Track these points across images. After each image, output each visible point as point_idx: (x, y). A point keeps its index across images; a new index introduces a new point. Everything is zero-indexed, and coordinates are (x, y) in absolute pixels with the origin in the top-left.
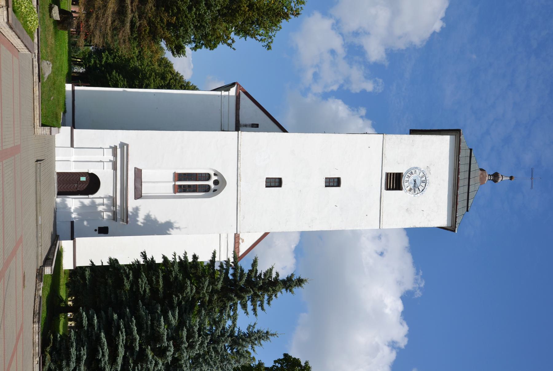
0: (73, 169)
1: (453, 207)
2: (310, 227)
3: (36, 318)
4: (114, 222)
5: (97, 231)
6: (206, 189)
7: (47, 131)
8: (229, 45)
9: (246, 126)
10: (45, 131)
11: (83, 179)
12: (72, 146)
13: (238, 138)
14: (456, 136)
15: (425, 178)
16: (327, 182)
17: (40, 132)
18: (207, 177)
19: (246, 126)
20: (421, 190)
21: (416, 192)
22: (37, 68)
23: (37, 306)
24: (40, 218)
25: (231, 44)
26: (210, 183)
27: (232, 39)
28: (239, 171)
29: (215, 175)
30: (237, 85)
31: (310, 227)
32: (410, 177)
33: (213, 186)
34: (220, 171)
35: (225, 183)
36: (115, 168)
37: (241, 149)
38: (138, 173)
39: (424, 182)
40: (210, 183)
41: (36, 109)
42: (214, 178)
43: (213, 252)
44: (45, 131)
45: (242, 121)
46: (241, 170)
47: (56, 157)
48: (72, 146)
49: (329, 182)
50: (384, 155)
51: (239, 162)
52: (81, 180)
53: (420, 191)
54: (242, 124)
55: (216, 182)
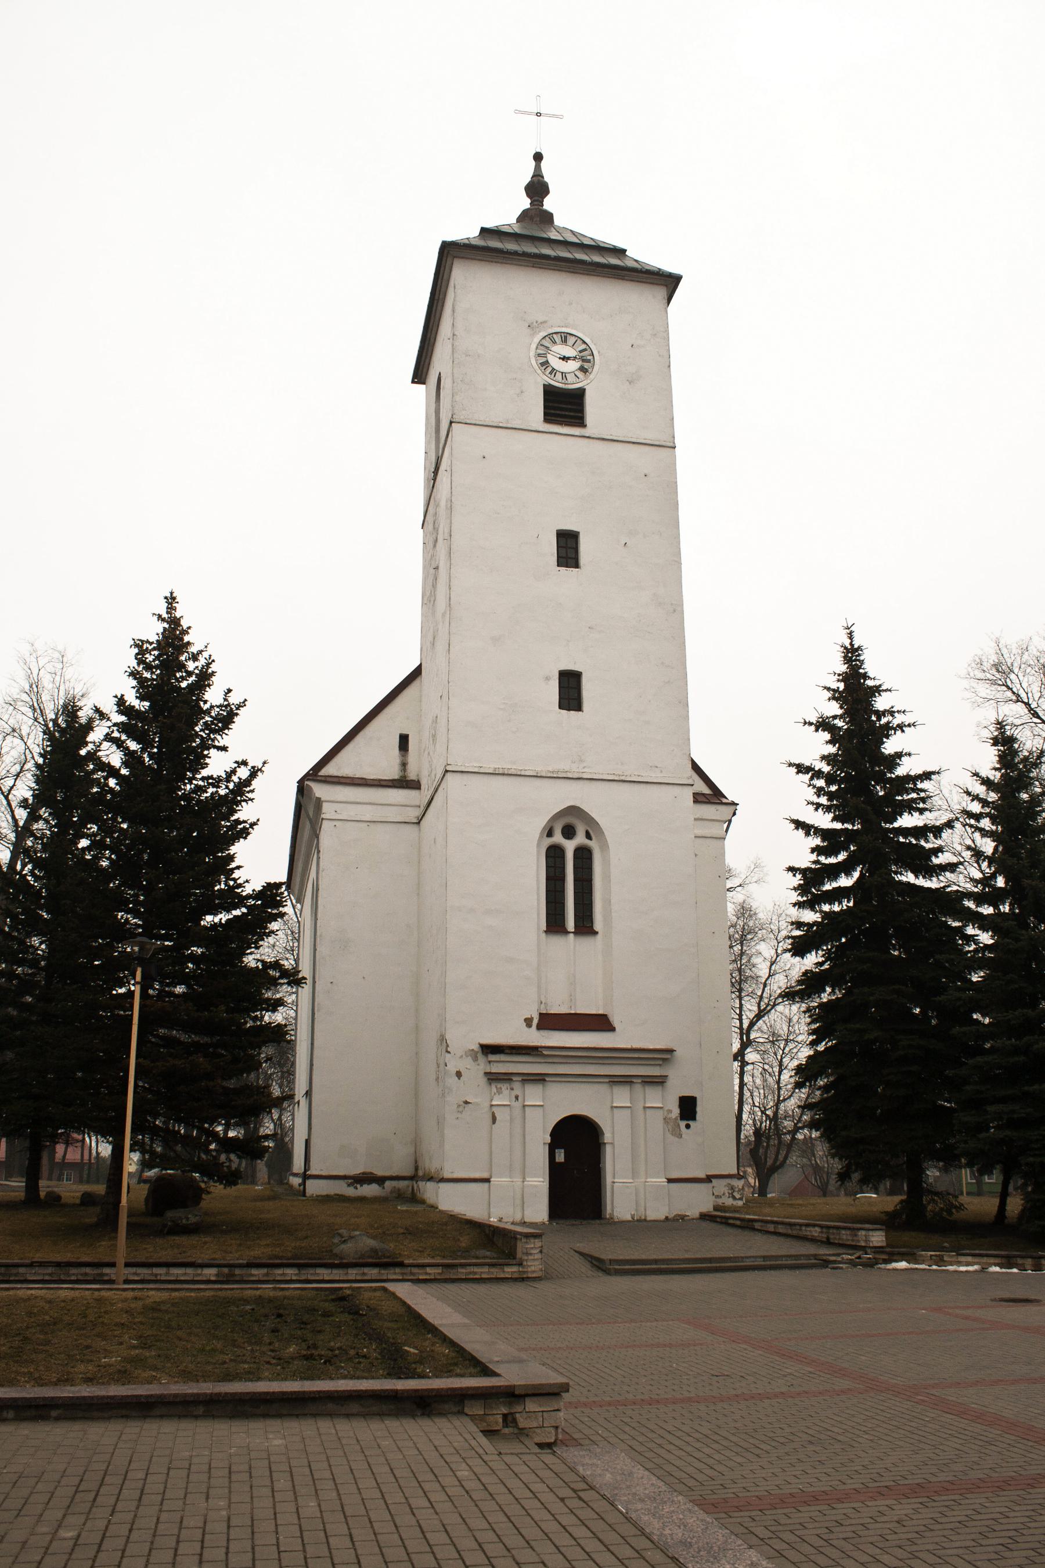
0: (539, 1182)
1: (622, 278)
2: (675, 611)
3: (69, 1275)
4: (669, 1083)
5: (690, 1123)
6: (584, 856)
7: (532, 1246)
8: (254, 773)
9: (404, 765)
10: (533, 1251)
11: (560, 1156)
12: (487, 1180)
13: (462, 772)
14: (455, 257)
15: (554, 336)
16: (567, 562)
17: (537, 1263)
18: (554, 855)
19: (404, 765)
20: (584, 346)
21: (588, 358)
22: (366, 1270)
23: (136, 1274)
24: (463, 1271)
25: (253, 767)
26: (570, 847)
27: (236, 765)
28: (544, 774)
29: (550, 834)
30: (308, 780)
31: (675, 611)
32: (553, 369)
33: (580, 839)
34: (542, 822)
35: (573, 811)
36: (540, 1079)
37: (489, 767)
38: (549, 1021)
39: (566, 337)
40: (570, 847)
41: (475, 1273)
42: (558, 838)
43: (793, 826)
44: (533, 1251)
45: (392, 772)
46: (541, 769)
47: (997, 1204)
48: (487, 1180)
49: (567, 558)
50: (501, 425)
51: (523, 773)
52: (563, 1160)
53: (585, 350)
54: (401, 774)
55: (569, 832)
